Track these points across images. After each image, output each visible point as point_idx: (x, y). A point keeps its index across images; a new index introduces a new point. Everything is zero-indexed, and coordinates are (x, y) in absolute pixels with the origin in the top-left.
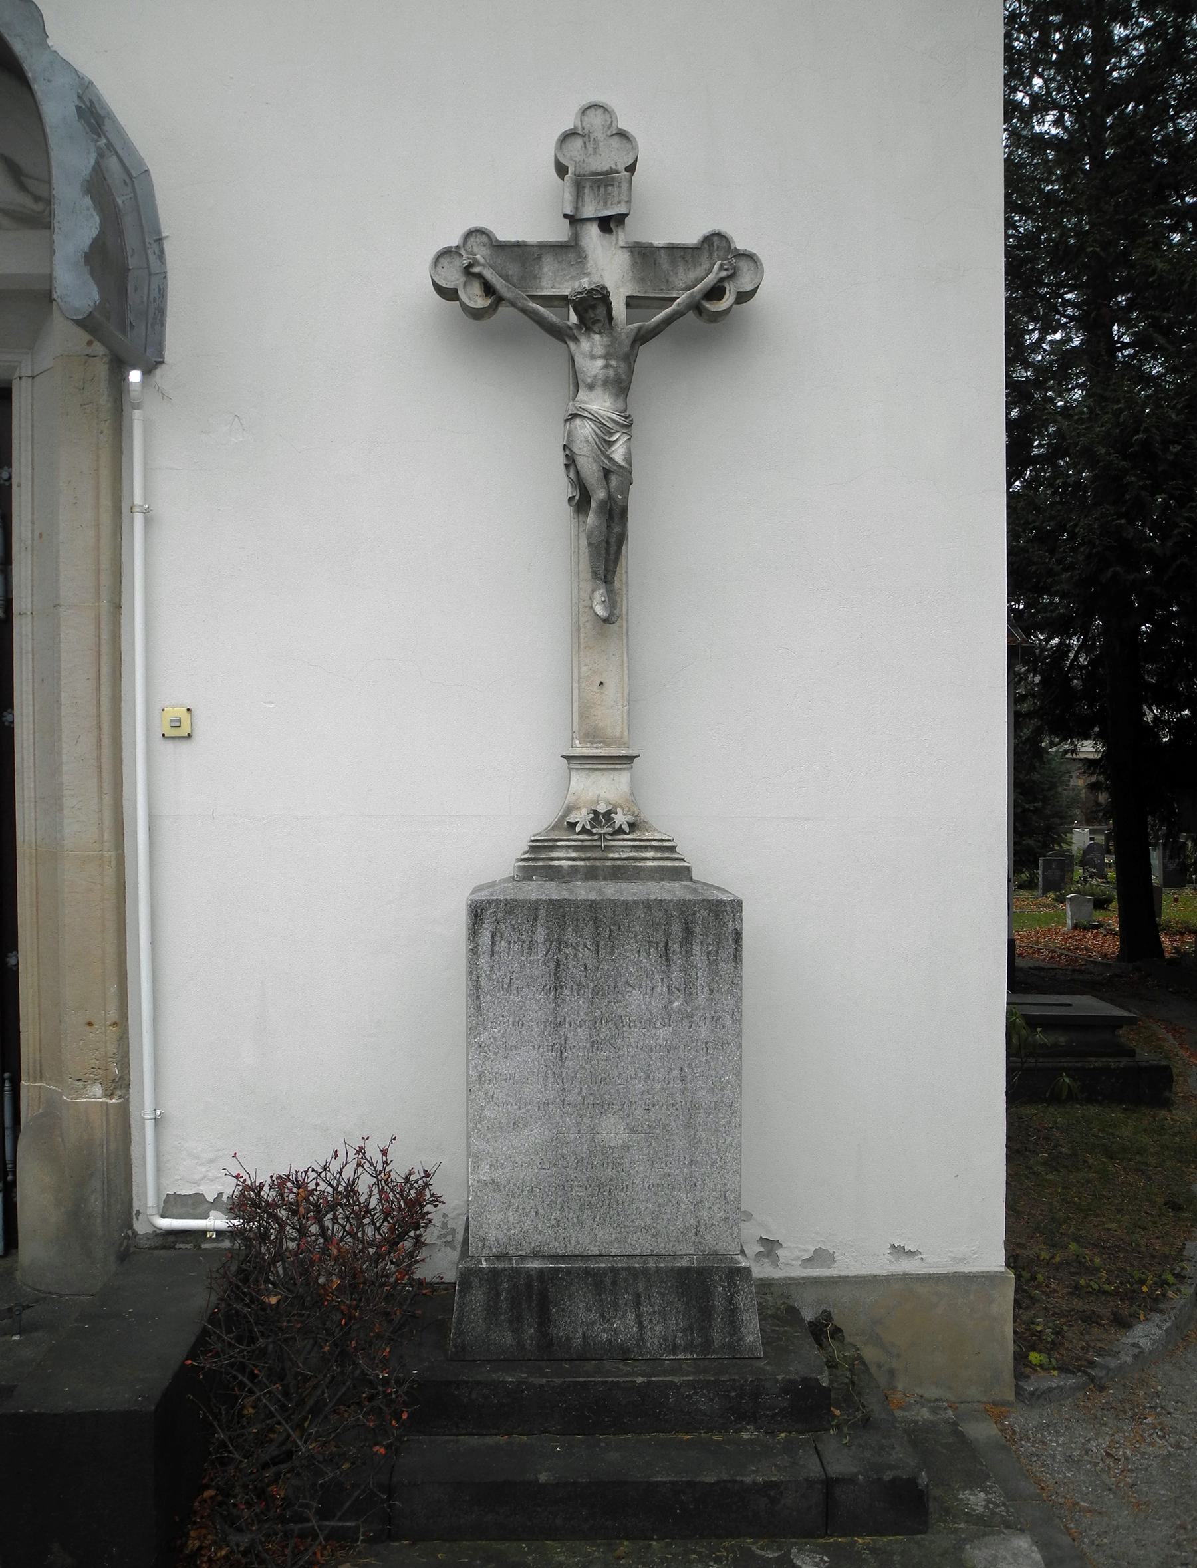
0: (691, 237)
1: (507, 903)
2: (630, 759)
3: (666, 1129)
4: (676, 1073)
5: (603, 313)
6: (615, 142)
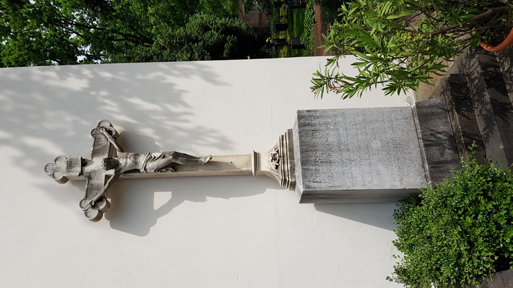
1: (303, 178)
2: (255, 153)
3: (373, 129)
4: (354, 127)
6: (57, 162)
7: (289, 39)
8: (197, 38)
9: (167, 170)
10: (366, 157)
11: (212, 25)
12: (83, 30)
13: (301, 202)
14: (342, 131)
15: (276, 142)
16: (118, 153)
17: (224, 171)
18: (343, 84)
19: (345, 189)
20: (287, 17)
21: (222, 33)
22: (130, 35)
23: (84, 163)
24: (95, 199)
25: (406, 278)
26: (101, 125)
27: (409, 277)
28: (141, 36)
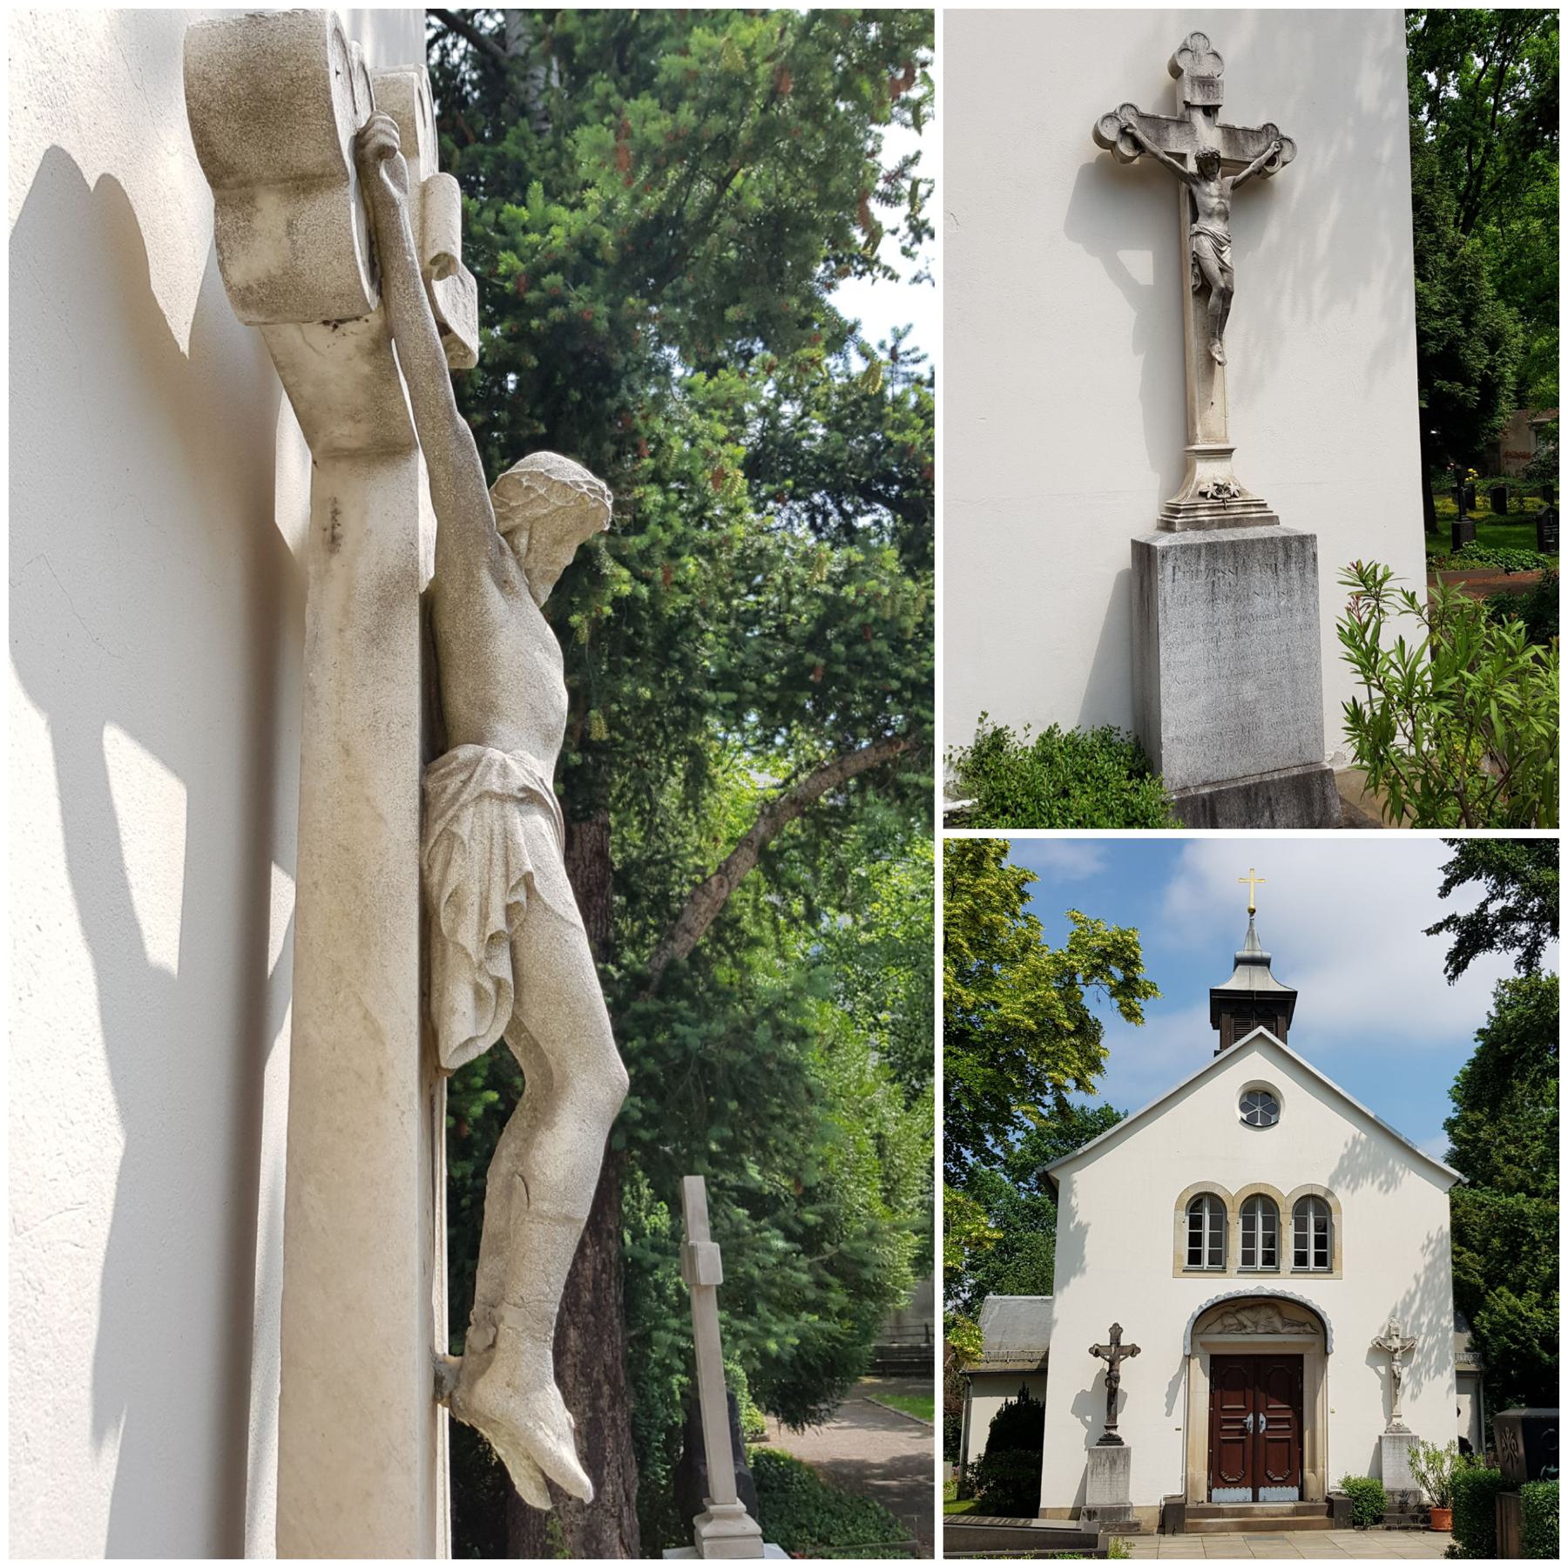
0: (1256, 124)
2: (1231, 451)
5: (1177, 174)
6: (1211, 58)
7: (1475, 515)
8: (1475, 324)
9: (1196, 277)
10: (1225, 672)
11: (1501, 356)
12: (1492, 84)
13: (1134, 543)
14: (1275, 622)
15: (1254, 493)
16: (1230, 178)
17: (1197, 390)
18: (1365, 619)
19: (1161, 629)
20: (1521, 512)
21: (1485, 377)
22: (1480, 182)
23: (1210, 111)
24: (1139, 134)
25: (985, 750)
26: (1285, 144)
27: (987, 755)
28: (1479, 205)
